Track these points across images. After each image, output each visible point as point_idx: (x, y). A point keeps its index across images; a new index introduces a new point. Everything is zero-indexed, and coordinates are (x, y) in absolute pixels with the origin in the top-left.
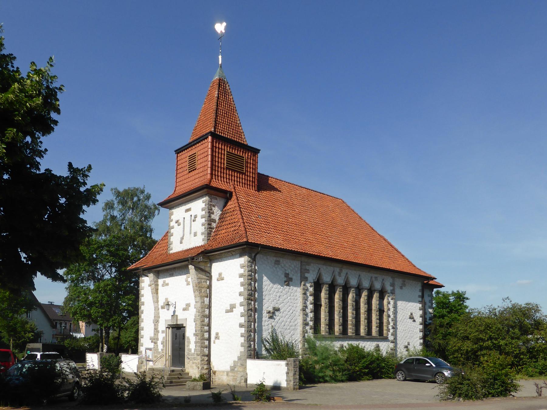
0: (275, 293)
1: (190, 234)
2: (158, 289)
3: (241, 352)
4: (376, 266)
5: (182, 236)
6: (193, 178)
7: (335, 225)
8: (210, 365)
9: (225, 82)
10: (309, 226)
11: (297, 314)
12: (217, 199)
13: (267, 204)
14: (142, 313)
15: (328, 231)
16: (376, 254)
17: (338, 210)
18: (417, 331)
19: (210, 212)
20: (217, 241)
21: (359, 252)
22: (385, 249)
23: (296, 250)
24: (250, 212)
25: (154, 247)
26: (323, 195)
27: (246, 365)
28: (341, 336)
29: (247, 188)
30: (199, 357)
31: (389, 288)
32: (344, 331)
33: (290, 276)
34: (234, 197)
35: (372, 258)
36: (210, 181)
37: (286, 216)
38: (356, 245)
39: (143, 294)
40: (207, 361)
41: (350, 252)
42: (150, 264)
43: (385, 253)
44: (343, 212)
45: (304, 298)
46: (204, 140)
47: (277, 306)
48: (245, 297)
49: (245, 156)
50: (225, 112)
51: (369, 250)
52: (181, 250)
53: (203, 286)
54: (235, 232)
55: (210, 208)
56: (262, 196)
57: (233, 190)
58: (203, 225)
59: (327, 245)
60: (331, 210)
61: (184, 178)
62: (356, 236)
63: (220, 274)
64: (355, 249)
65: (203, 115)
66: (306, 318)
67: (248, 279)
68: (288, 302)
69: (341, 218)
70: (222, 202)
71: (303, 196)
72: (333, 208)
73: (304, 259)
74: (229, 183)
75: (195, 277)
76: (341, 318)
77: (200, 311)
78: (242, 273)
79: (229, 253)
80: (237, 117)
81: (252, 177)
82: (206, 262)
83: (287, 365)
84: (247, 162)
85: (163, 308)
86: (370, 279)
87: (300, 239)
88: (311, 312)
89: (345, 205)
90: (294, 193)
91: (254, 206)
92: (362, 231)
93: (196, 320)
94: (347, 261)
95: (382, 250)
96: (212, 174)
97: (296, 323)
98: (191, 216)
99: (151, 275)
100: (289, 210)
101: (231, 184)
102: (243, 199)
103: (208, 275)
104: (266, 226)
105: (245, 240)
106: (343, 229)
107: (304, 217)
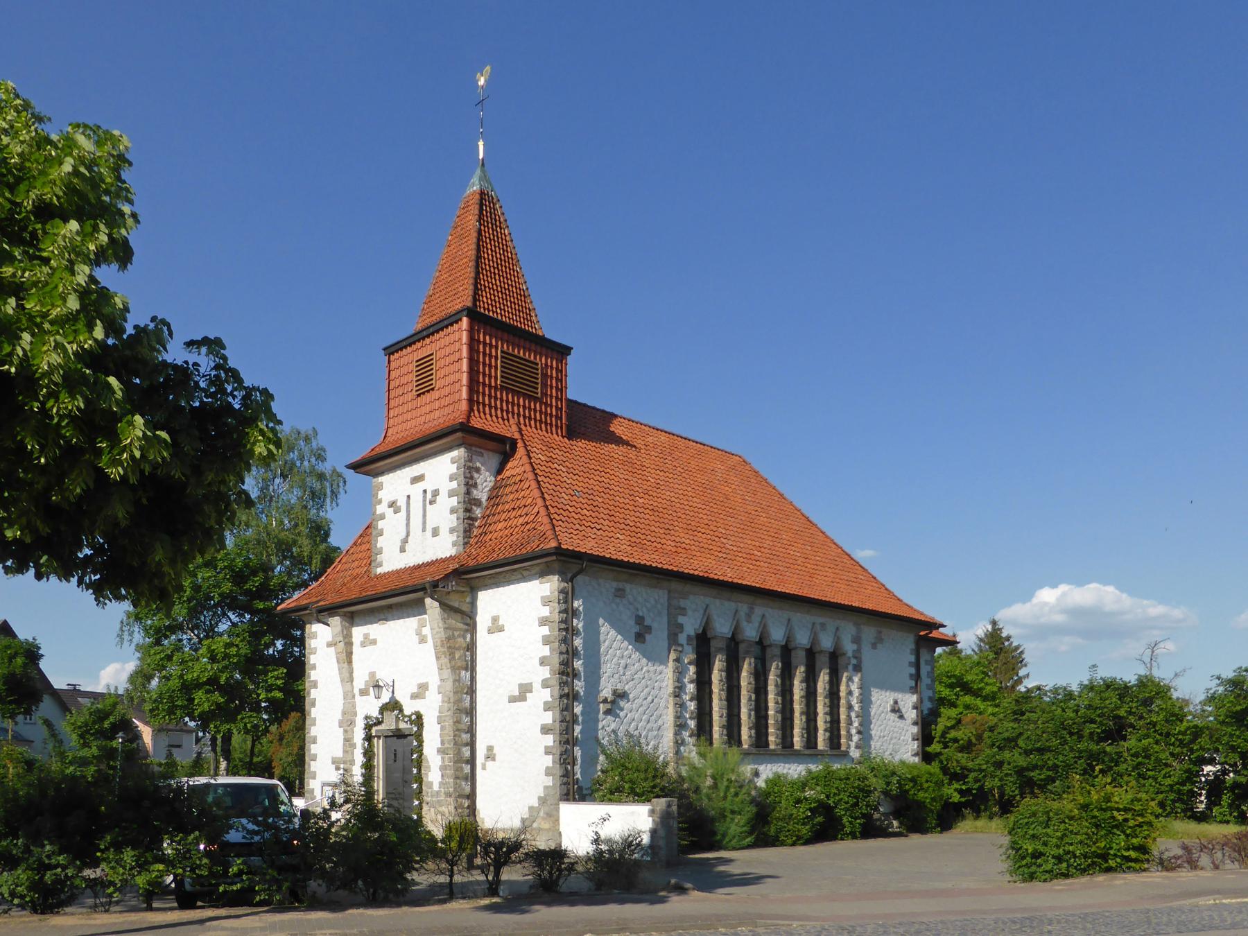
0: (616, 659)
1: (424, 529)
2: (351, 653)
3: (546, 788)
4: (824, 599)
5: (403, 535)
6: (428, 408)
7: (731, 511)
8: (475, 816)
9: (493, 198)
10: (679, 514)
11: (663, 704)
12: (482, 455)
13: (591, 467)
14: (313, 704)
15: (719, 525)
16: (821, 573)
17: (735, 479)
18: (906, 738)
19: (470, 486)
20: (488, 546)
21: (786, 569)
22: (837, 563)
23: (660, 566)
24: (556, 483)
25: (338, 560)
26: (702, 446)
27: (559, 817)
28: (754, 750)
29: (557, 434)
30: (451, 800)
31: (849, 647)
32: (760, 740)
33: (648, 622)
34: (521, 451)
35: (813, 583)
36: (469, 416)
37: (632, 492)
38: (778, 553)
39: (315, 664)
40: (468, 807)
41: (767, 570)
42: (331, 599)
43: (837, 571)
44: (746, 483)
45: (677, 668)
46: (452, 324)
47: (619, 686)
48: (555, 668)
49: (541, 360)
50: (495, 265)
52: (403, 567)
53: (457, 646)
54: (528, 527)
55: (469, 475)
56: (577, 449)
57: (517, 436)
58: (453, 511)
59: (720, 555)
60: (721, 479)
61: (405, 408)
62: (776, 535)
63: (495, 619)
64: (777, 562)
65: (447, 270)
66: (681, 712)
67: (560, 629)
68: (643, 678)
69: (743, 497)
70: (494, 460)
71: (661, 448)
72: (724, 476)
73: (675, 585)
74: (508, 421)
75: (440, 625)
76: (753, 713)
77: (452, 701)
78: (547, 617)
79: (515, 573)
80: (520, 275)
81: (557, 407)
82: (463, 592)
83: (652, 812)
84: (545, 376)
85: (364, 692)
86: (810, 626)
87: (663, 541)
88: (691, 700)
89: (747, 467)
90: (643, 443)
91: (564, 470)
92: (787, 525)
93: (443, 719)
94: (764, 589)
95: (832, 566)
96: (471, 401)
97: (660, 722)
98: (425, 491)
99: (336, 621)
100: (635, 479)
101: (512, 421)
102: (540, 456)
103: (468, 621)
104: (593, 515)
105: (553, 544)
106: (748, 520)
107: (668, 493)
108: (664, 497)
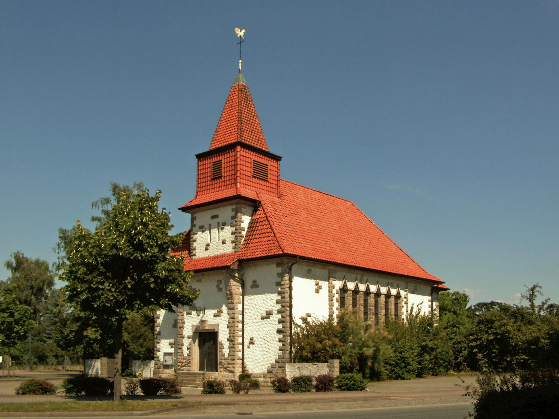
7: (350, 230)
37: (309, 224)
51: (384, 255)
59: (348, 252)
73: (331, 267)
87: (325, 247)
98: (219, 223)
108: (322, 225)
